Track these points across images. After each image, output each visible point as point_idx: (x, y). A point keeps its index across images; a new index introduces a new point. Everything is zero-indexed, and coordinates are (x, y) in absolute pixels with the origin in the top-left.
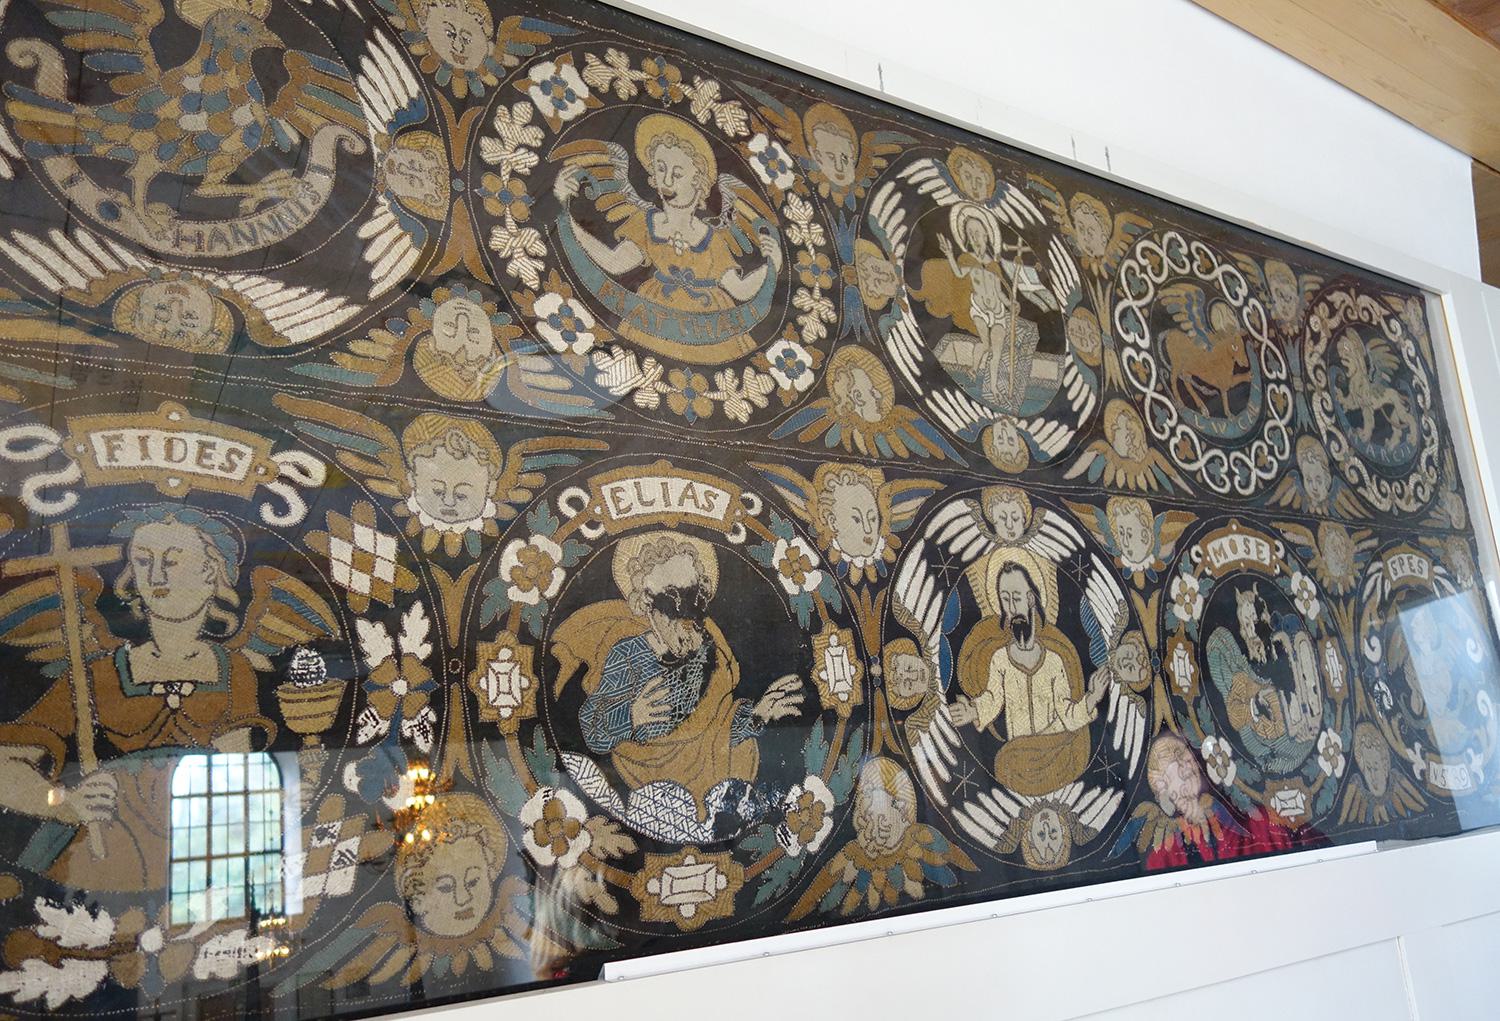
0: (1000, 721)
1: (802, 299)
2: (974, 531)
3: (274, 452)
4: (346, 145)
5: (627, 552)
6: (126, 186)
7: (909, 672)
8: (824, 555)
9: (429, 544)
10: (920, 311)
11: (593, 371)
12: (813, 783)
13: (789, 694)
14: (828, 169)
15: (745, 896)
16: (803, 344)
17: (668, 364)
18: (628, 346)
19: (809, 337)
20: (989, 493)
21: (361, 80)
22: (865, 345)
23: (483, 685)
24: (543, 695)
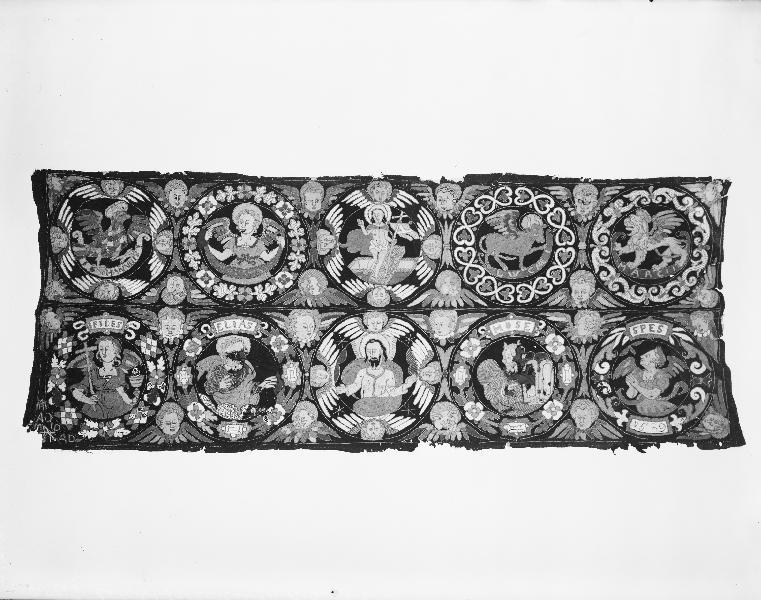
0: (358, 394)
1: (292, 256)
2: (358, 328)
5: (220, 341)
6: (96, 263)
7: (319, 376)
9: (165, 342)
10: (344, 251)
11: (213, 291)
15: (251, 434)
16: (290, 272)
17: (238, 286)
18: (224, 282)
19: (292, 269)
20: (367, 315)
22: (317, 268)
24: (194, 380)
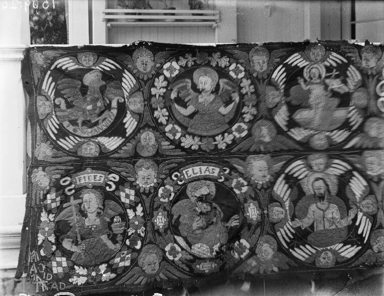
0: (312, 227)
1: (245, 109)
3: (109, 174)
4: (120, 101)
6: (77, 125)
8: (249, 182)
9: (142, 191)
10: (288, 104)
11: (180, 142)
12: (243, 241)
13: (236, 220)
14: (257, 68)
16: (244, 122)
18: (190, 134)
19: (247, 120)
21: (342, 245)
23: (155, 221)
24: (170, 222)
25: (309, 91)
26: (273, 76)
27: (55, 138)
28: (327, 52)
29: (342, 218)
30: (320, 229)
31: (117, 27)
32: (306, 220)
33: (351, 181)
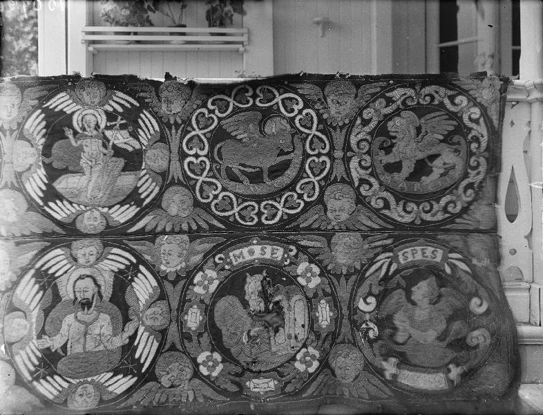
10: (48, 167)
25: (81, 149)
26: (27, 126)
27: (41, 204)
28: (109, 92)
29: (115, 335)
30: (77, 351)
31: (106, 51)
32: (58, 337)
33: (135, 279)
